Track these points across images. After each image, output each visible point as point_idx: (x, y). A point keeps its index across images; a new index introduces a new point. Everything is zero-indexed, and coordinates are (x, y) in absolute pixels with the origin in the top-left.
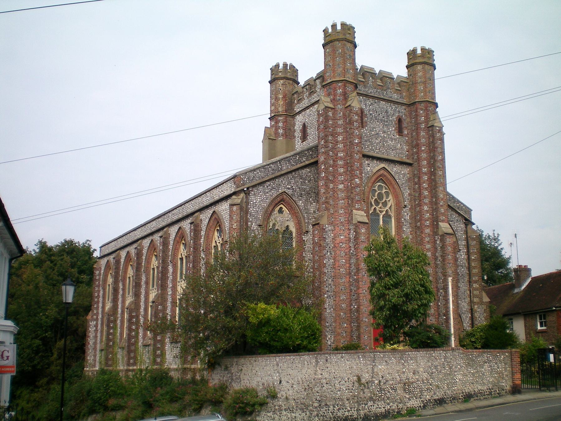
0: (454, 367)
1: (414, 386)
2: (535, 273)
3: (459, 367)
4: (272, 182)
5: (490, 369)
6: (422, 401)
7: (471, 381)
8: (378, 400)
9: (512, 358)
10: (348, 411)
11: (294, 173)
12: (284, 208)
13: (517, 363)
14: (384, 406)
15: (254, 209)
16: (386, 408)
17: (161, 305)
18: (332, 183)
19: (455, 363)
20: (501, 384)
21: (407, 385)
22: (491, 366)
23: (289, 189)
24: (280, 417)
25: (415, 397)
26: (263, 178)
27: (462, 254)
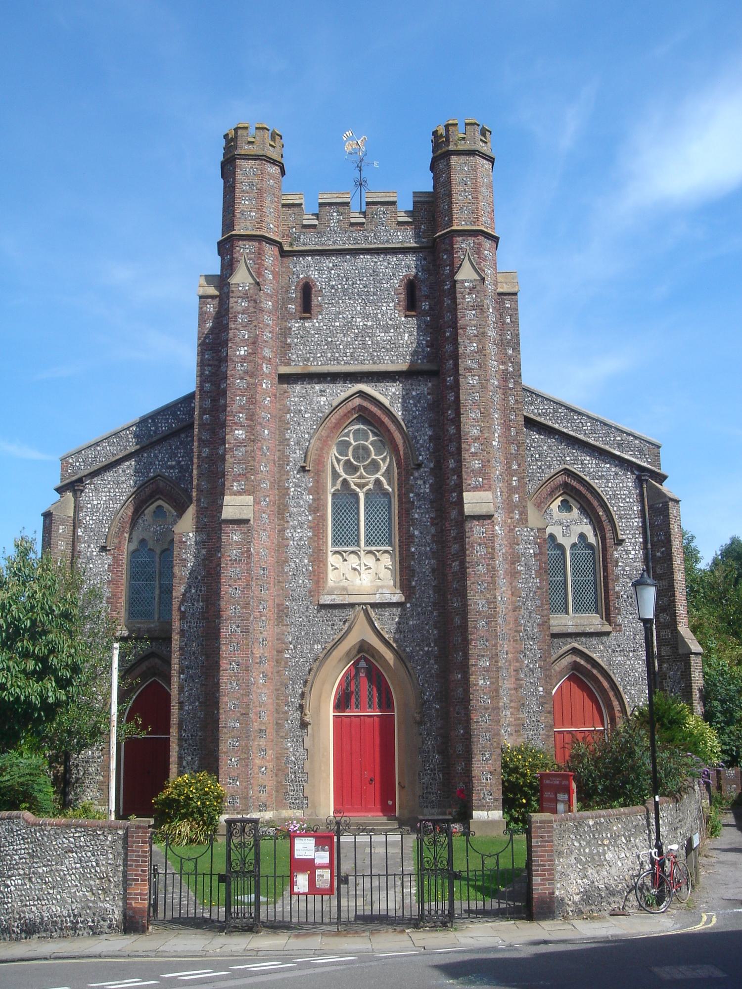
11: (183, 436)
12: (166, 506)
13: (136, 851)
15: (94, 518)
18: (207, 447)
20: (101, 905)
23: (172, 467)
26: (114, 455)
27: (630, 548)
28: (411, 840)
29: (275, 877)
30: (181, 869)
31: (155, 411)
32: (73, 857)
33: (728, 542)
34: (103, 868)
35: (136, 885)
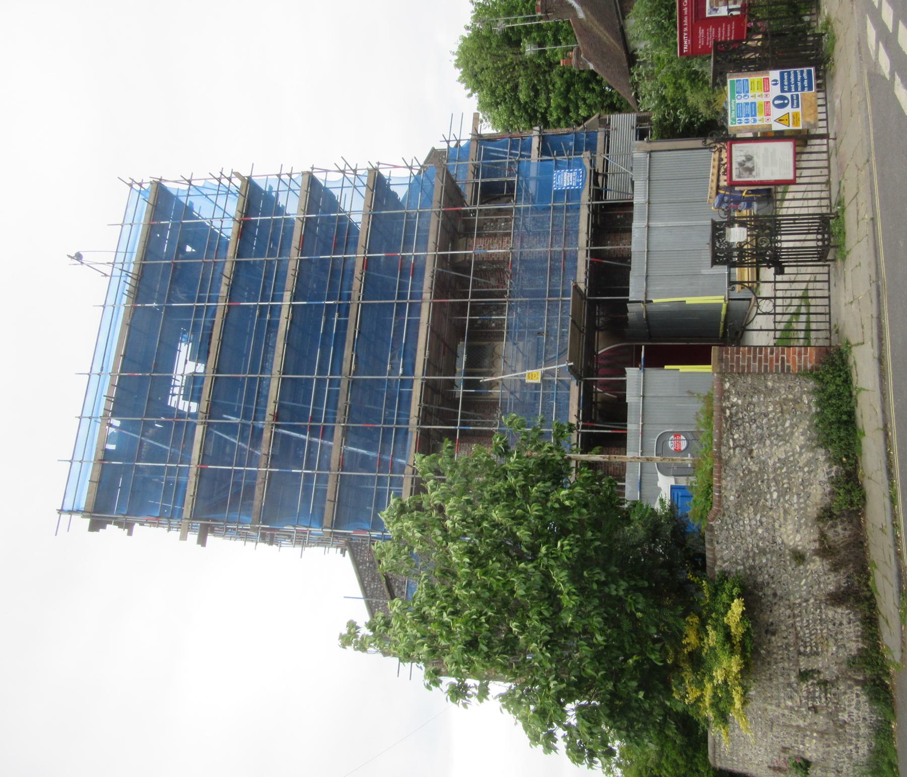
4: (395, 583)
5: (768, 442)
6: (849, 623)
7: (802, 500)
13: (755, 358)
14: (855, 695)
21: (802, 649)
22: (761, 439)
28: (728, 75)
29: (775, 314)
30: (769, 314)
31: (356, 572)
32: (758, 448)
33: (212, 539)
34: (771, 409)
35: (788, 361)
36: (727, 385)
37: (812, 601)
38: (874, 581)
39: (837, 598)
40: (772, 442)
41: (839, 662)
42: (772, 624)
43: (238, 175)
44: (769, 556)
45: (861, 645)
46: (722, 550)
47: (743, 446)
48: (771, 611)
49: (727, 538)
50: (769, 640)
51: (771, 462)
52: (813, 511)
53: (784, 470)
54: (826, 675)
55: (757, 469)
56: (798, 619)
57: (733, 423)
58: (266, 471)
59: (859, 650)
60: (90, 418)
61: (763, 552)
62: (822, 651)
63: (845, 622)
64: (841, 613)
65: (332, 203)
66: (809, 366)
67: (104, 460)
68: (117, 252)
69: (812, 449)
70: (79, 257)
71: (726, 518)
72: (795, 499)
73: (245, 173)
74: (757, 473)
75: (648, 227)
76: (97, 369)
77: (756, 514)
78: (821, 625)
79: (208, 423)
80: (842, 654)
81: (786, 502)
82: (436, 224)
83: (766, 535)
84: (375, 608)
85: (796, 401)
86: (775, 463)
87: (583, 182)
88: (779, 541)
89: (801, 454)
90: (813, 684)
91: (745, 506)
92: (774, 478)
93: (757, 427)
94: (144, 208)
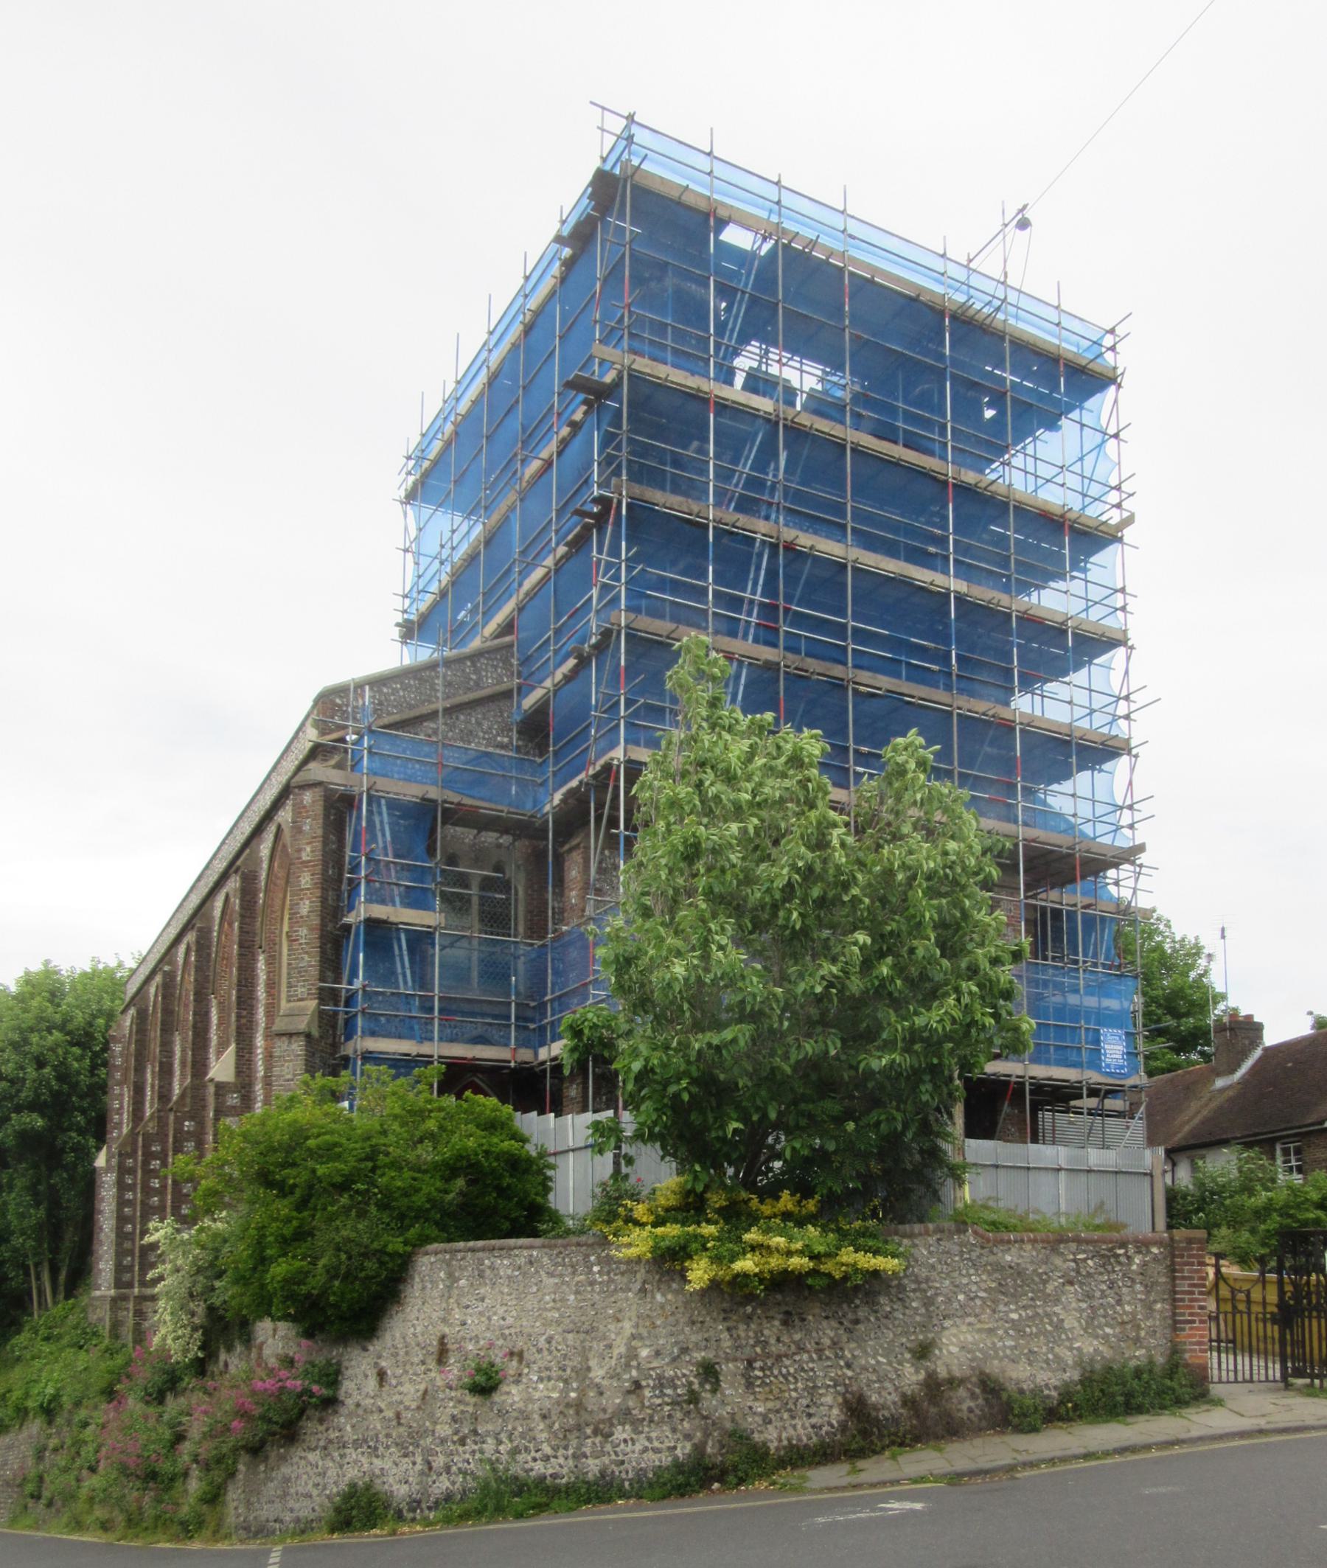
0: (940, 1299)
1: (784, 1371)
2: (1271, 1037)
3: (961, 1297)
5: (1084, 1305)
6: (813, 1427)
7: (1008, 1352)
8: (651, 1421)
9: (1173, 1263)
10: (546, 1459)
16: (679, 1452)
17: (191, 1118)
19: (947, 1282)
21: (758, 1364)
22: (1089, 1296)
24: (341, 1466)
25: (790, 1410)
26: (411, 707)
34: (1127, 1308)
35: (1191, 1329)
36: (1155, 1250)
37: (849, 1373)
38: (921, 1449)
39: (857, 1408)
40: (1083, 1310)
41: (737, 1418)
42: (803, 1320)
43: (1129, 521)
44: (923, 1311)
45: (773, 1446)
46: (928, 1246)
47: (1078, 1272)
48: (827, 1318)
49: (948, 1253)
50: (773, 1318)
51: (1057, 1309)
52: (994, 1367)
53: (1049, 1328)
54: (709, 1402)
55: (1048, 1291)
56: (815, 1356)
57: (1108, 1259)
58: (707, 519)
59: (764, 1444)
60: (778, 203)
61: (928, 1302)
62: (754, 1393)
63: (813, 1420)
64: (831, 1412)
65: (1058, 670)
66: (1187, 1356)
67: (715, 217)
68: (1020, 291)
69: (1079, 1363)
70: (1024, 224)
71: (978, 1251)
72: (1010, 1343)
73: (1128, 534)
74: (1043, 1291)
75: (1059, 1170)
76: (853, 228)
77: (985, 1291)
78: (804, 1390)
79: (777, 423)
80: (751, 1422)
81: (1006, 1332)
82: (1058, 842)
83: (956, 1305)
84: (402, 683)
85: (1137, 1341)
86: (1056, 1314)
87: (1110, 1074)
88: (947, 1323)
89: (1071, 1349)
90: (690, 1384)
91: (997, 1275)
92: (1038, 1314)
93: (1103, 1291)
94: (1070, 346)
